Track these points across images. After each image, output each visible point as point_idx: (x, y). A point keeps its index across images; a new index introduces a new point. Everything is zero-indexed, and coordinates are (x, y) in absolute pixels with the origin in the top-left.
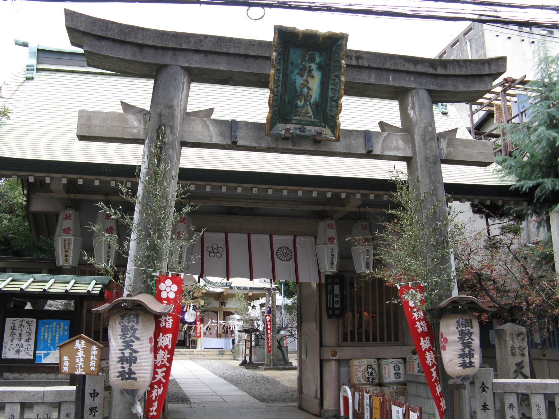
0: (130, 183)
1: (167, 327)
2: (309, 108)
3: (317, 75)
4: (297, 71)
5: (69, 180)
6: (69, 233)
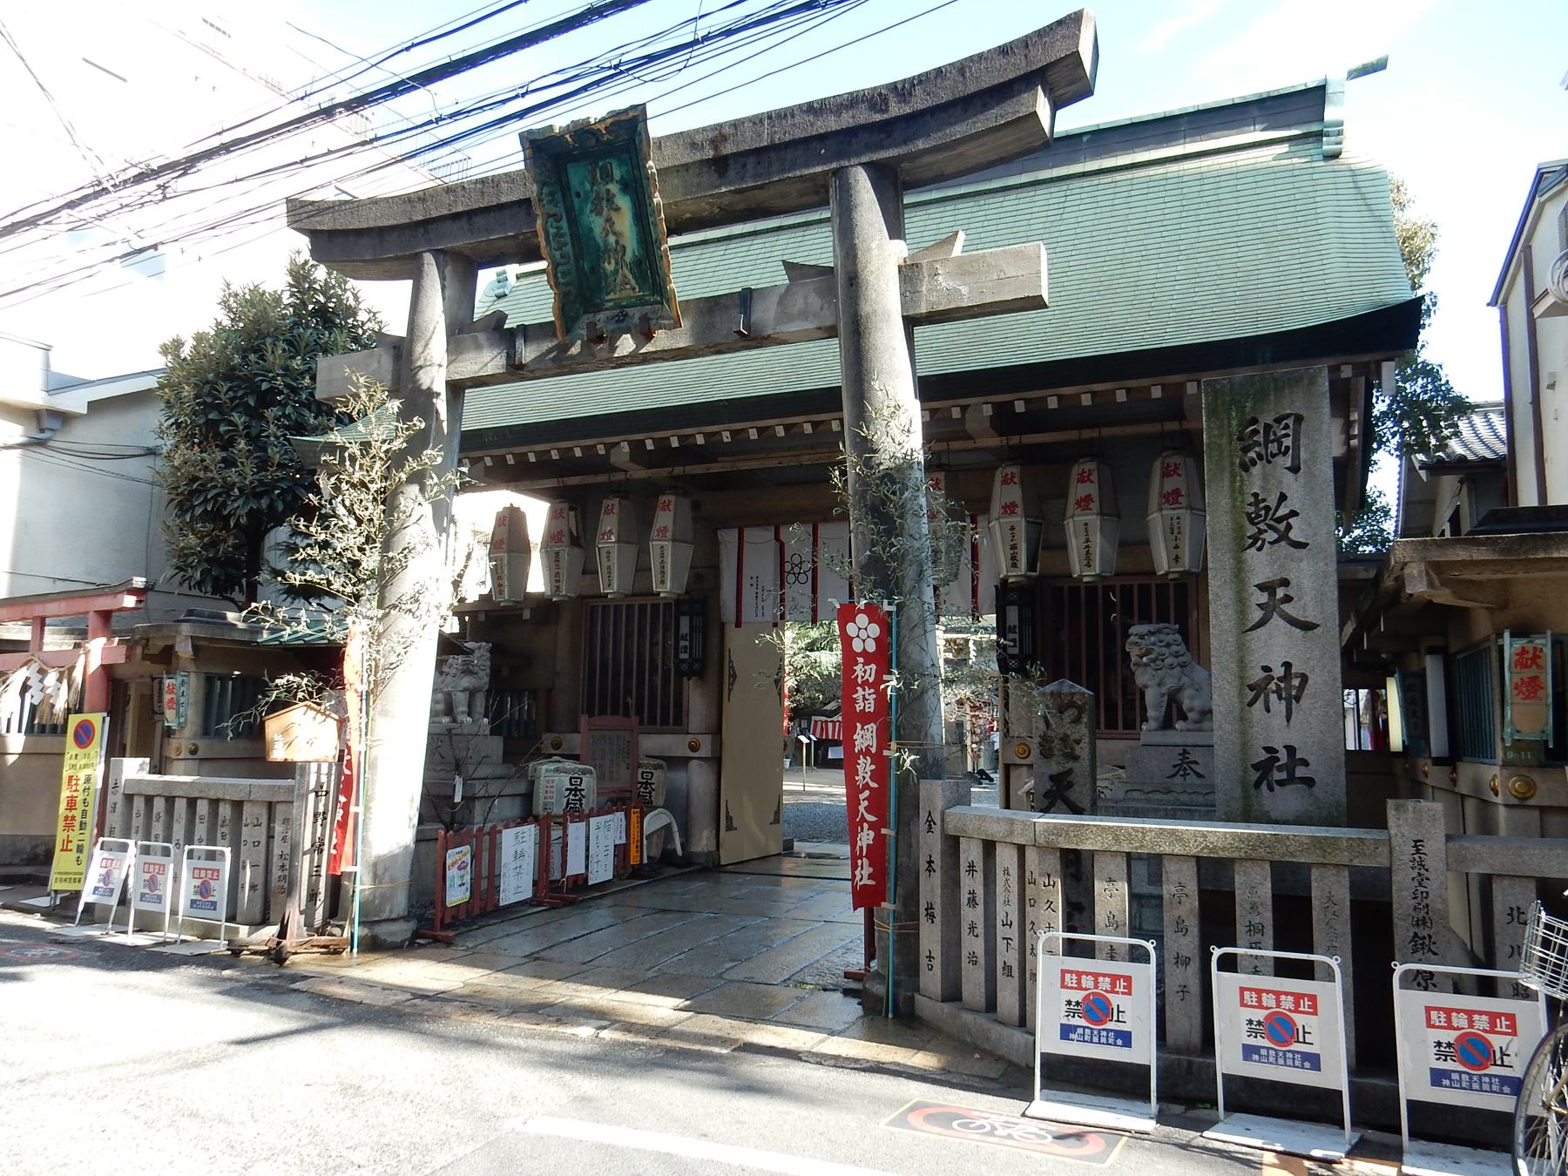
0: (1055, 398)
1: (867, 710)
2: (627, 272)
3: (624, 202)
4: (589, 206)
5: (997, 407)
6: (1177, 502)
